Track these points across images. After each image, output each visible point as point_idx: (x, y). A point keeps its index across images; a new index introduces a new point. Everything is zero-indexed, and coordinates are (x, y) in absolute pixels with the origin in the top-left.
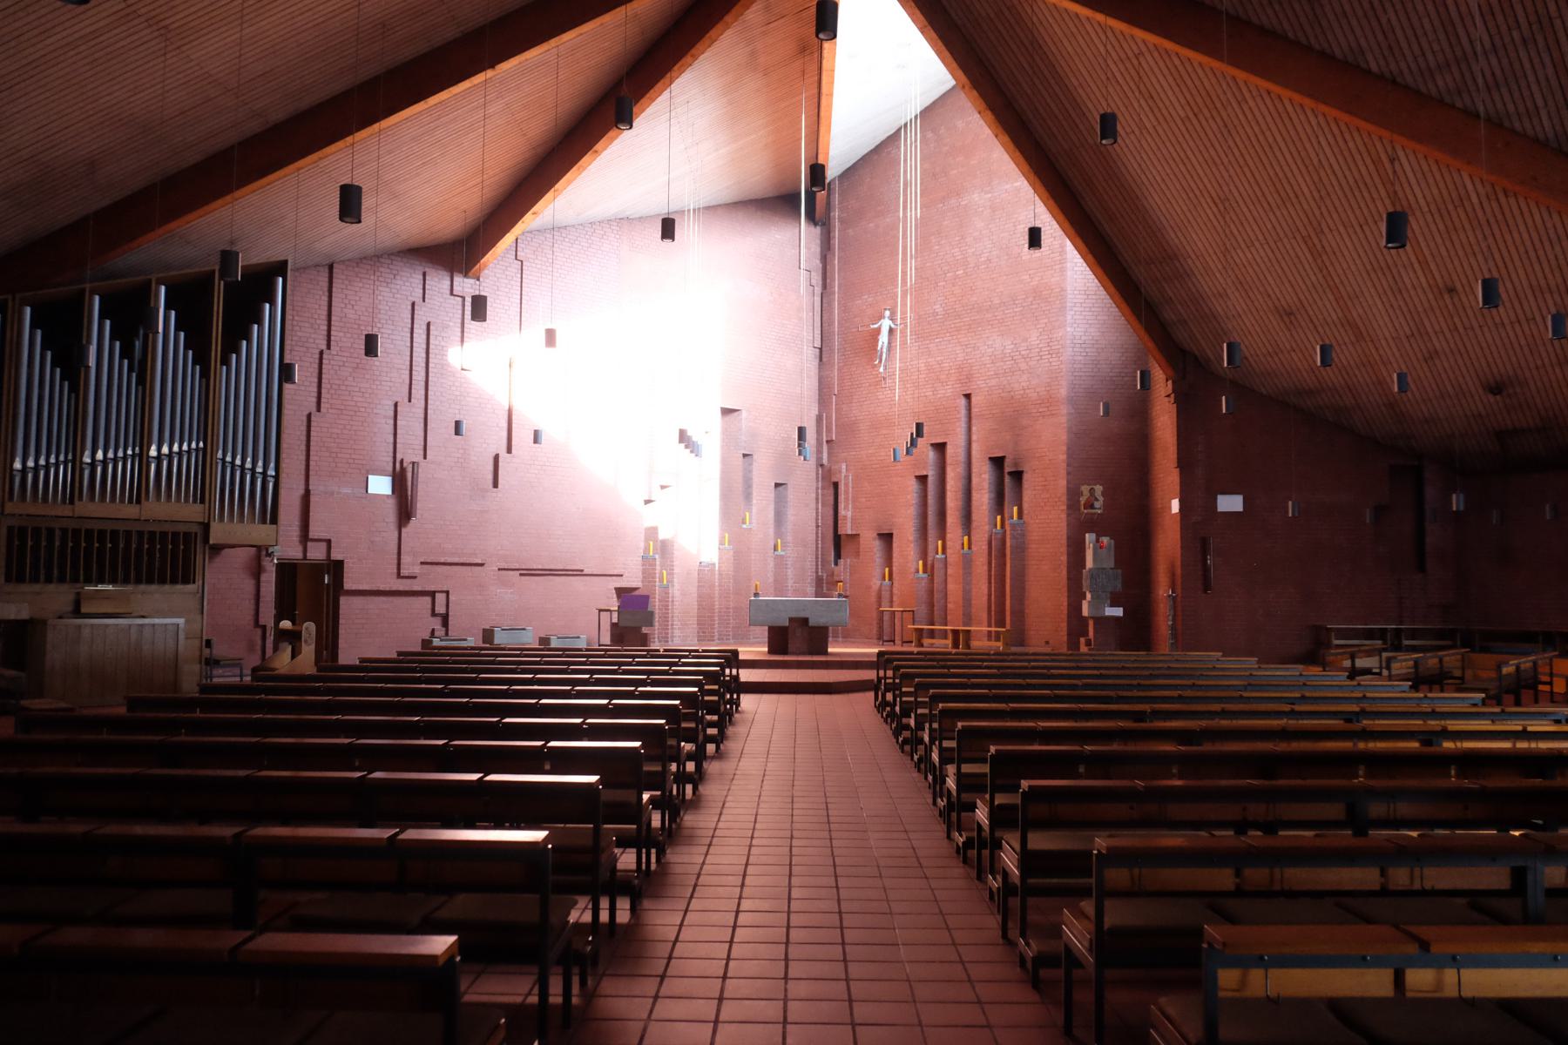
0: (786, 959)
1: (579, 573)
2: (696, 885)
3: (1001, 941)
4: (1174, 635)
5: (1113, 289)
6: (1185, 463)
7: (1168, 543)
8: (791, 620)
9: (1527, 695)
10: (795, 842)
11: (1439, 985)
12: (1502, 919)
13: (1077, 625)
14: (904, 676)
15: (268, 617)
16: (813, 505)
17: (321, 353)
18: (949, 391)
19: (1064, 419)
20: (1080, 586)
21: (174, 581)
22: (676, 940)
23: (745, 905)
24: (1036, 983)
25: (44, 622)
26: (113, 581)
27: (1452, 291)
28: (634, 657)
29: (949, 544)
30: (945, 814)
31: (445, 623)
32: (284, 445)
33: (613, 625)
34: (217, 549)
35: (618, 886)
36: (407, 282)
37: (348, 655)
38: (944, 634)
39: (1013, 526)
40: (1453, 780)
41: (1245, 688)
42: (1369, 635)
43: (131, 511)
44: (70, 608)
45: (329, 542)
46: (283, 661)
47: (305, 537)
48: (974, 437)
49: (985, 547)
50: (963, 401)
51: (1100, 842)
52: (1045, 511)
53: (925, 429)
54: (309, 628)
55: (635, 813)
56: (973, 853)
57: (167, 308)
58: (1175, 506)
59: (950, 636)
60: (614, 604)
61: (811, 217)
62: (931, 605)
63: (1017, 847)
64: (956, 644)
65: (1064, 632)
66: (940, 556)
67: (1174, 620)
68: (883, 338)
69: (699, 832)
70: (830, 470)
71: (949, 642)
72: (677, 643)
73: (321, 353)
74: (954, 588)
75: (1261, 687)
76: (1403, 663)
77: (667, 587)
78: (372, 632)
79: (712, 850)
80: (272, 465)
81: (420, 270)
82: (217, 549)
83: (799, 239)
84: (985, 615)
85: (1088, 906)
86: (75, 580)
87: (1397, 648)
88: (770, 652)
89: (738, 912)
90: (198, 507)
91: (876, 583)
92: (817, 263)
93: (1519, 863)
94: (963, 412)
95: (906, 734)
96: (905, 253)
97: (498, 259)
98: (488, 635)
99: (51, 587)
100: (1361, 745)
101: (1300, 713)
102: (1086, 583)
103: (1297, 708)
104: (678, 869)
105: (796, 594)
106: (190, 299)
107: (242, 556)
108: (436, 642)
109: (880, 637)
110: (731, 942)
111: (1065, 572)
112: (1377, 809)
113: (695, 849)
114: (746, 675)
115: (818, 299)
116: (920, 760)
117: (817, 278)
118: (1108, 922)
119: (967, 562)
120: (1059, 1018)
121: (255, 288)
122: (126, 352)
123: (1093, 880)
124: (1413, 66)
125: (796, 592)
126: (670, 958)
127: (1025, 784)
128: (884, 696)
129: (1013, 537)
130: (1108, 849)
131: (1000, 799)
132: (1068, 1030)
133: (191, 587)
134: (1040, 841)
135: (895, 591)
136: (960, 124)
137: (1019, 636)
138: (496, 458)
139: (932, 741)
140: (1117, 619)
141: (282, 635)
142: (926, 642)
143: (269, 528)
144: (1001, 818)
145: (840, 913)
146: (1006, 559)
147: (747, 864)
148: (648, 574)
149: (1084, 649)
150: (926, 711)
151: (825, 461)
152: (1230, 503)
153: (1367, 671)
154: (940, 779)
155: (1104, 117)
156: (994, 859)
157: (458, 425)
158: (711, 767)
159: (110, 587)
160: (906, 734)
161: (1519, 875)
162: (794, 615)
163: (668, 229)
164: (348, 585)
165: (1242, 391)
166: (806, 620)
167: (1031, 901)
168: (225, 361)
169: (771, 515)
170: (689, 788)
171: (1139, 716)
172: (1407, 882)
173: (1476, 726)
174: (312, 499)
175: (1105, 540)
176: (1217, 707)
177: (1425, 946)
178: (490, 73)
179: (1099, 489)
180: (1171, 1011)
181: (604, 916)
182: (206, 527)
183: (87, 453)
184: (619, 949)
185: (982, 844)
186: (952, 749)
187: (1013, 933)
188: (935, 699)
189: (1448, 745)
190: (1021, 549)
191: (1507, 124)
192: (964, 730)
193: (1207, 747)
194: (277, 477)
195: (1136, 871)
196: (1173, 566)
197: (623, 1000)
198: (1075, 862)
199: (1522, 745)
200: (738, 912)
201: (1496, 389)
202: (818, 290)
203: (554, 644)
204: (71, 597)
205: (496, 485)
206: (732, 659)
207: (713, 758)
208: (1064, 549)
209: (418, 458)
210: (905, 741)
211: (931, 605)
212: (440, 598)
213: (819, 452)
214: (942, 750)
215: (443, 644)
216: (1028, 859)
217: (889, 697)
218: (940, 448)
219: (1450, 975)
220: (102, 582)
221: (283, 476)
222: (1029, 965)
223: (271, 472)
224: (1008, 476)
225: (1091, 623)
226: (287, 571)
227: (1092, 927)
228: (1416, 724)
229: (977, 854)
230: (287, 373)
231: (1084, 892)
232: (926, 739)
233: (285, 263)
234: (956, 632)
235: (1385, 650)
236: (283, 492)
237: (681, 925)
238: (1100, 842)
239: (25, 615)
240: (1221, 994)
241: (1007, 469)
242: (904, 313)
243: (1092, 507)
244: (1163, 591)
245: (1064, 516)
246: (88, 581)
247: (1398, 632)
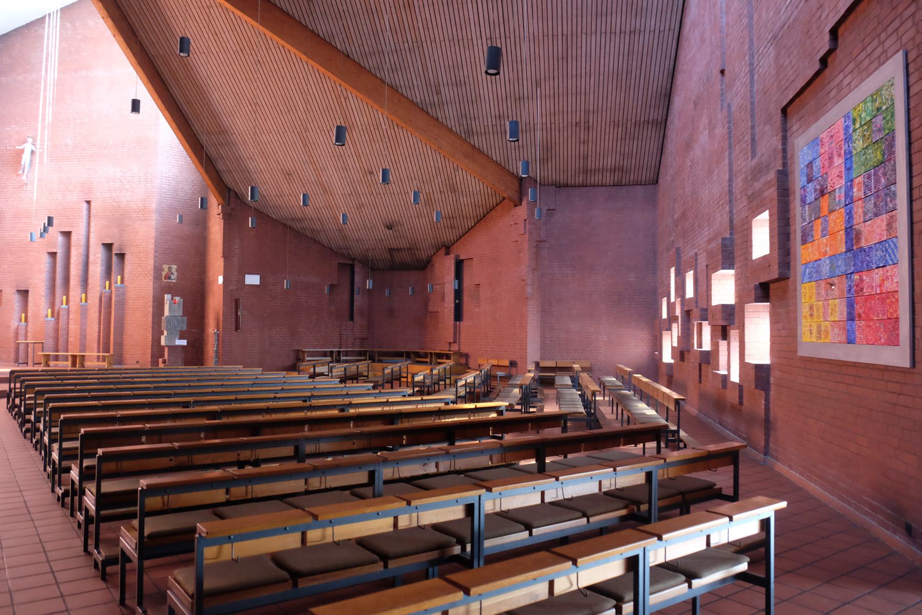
3: (83, 553)
4: (217, 356)
5: (188, 147)
6: (227, 255)
7: (216, 302)
9: (396, 383)
11: (324, 537)
12: (362, 497)
13: (157, 351)
14: (27, 387)
18: (75, 199)
19: (154, 223)
20: (160, 326)
24: (104, 577)
27: (371, 173)
29: (71, 298)
30: (51, 477)
38: (66, 358)
39: (117, 288)
40: (352, 428)
41: (252, 385)
42: (325, 354)
48: (92, 229)
49: (97, 301)
50: (85, 205)
51: (144, 482)
52: (139, 280)
53: (55, 222)
56: (68, 500)
58: (221, 280)
59: (70, 359)
62: (57, 339)
63: (94, 490)
64: (74, 364)
65: (149, 355)
66: (64, 306)
67: (218, 347)
68: (26, 157)
71: (69, 363)
74: (74, 327)
75: (261, 385)
76: (339, 370)
84: (96, 345)
85: (135, 523)
87: (338, 361)
91: (14, 324)
93: (372, 469)
94: (85, 212)
95: (28, 425)
96: (45, 101)
100: (309, 414)
101: (279, 398)
102: (164, 325)
103: (278, 396)
109: (16, 361)
111: (150, 318)
112: (310, 448)
116: (37, 442)
118: (147, 532)
119: (84, 311)
120: (117, 595)
123: (138, 508)
124: (358, 50)
127: (100, 451)
128: (14, 401)
129: (116, 296)
130: (148, 486)
131: (87, 463)
132: (122, 602)
134: (109, 486)
135: (29, 329)
136: (91, 23)
137: (119, 358)
139: (45, 429)
140: (183, 347)
142: (52, 363)
144: (85, 475)
146: (111, 311)
149: (161, 365)
150: (42, 409)
152: (253, 280)
153: (322, 374)
154: (48, 453)
155: (182, 39)
156: (81, 501)
160: (28, 425)
161: (372, 475)
165: (261, 215)
167: (103, 525)
171: (186, 405)
172: (318, 485)
173: (367, 400)
175: (177, 299)
176: (233, 397)
177: (315, 517)
179: (174, 267)
180: (180, 578)
181: (498, 501)
185: (74, 493)
186: (56, 433)
187: (91, 548)
188: (48, 400)
189: (352, 411)
190: (122, 303)
191: (400, 90)
192: (65, 420)
193: (224, 420)
195: (166, 497)
196: (218, 315)
198: (128, 497)
199: (386, 409)
201: (390, 227)
208: (151, 304)
210: (27, 431)
211: (57, 339)
214: (50, 434)
216: (103, 500)
217: (17, 401)
218: (67, 235)
219: (329, 530)
222: (100, 566)
224: (115, 255)
225: (166, 349)
227: (137, 534)
228: (339, 401)
229: (70, 499)
231: (132, 516)
232: (42, 427)
234: (74, 357)
235: (331, 362)
238: (144, 482)
240: (205, 562)
241: (115, 251)
242: (42, 141)
243: (169, 278)
244: (211, 329)
245: (151, 283)
247: (339, 352)
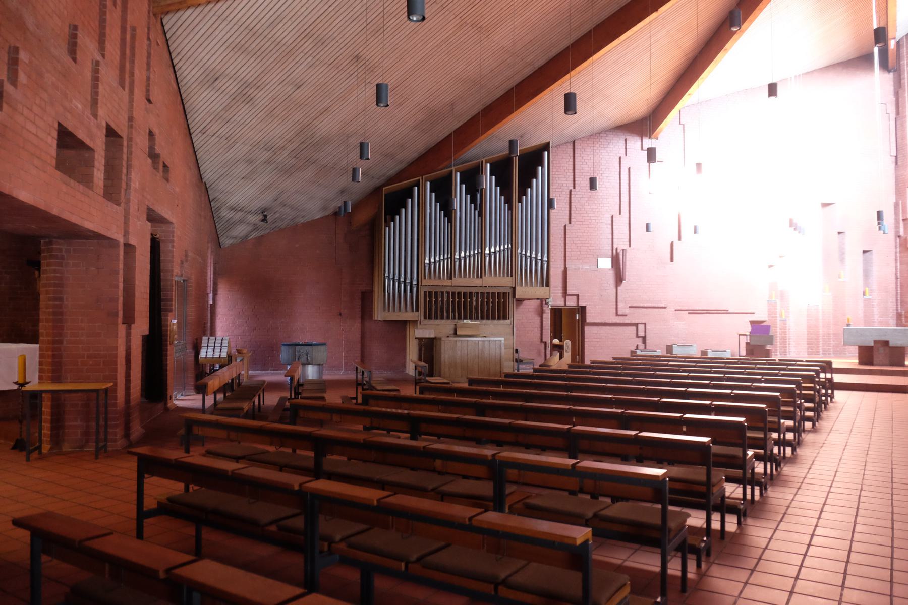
0: (845, 573)
1: (726, 312)
2: (785, 514)
8: (875, 342)
10: (863, 493)
15: (547, 337)
16: (893, 264)
17: (570, 191)
21: (499, 318)
22: (766, 548)
23: (819, 531)
25: (440, 339)
26: (471, 318)
28: (745, 368)
31: (644, 342)
32: (551, 244)
33: (747, 344)
34: (520, 301)
35: (725, 507)
36: (617, 145)
37: (590, 357)
43: (477, 282)
44: (452, 332)
45: (578, 296)
46: (555, 362)
47: (565, 294)
54: (567, 344)
55: (741, 463)
57: (461, 183)
60: (748, 329)
61: (884, 65)
69: (792, 479)
70: (906, 240)
72: (792, 355)
73: (570, 191)
77: (785, 320)
78: (603, 346)
79: (800, 492)
80: (546, 255)
81: (624, 137)
82: (520, 301)
83: (878, 81)
86: (454, 318)
88: (860, 363)
89: (813, 535)
90: (510, 279)
92: (892, 98)
97: (669, 124)
98: (669, 349)
99: (443, 321)
104: (774, 501)
105: (881, 323)
106: (501, 169)
107: (534, 304)
108: (639, 353)
110: (805, 555)
113: (787, 490)
114: (838, 378)
115: (893, 123)
117: (892, 109)
121: (533, 159)
122: (473, 200)
125: (881, 323)
126: (760, 559)
133: (507, 321)
138: (672, 244)
141: (555, 347)
143: (545, 289)
145: (892, 547)
147: (824, 504)
148: (772, 312)
151: (902, 233)
157: (648, 225)
158: (807, 437)
159: (469, 321)
162: (877, 339)
163: (772, 90)
164: (588, 320)
166: (886, 343)
168: (520, 201)
170: (789, 450)
174: (568, 272)
178: (654, 15)
182: (514, 289)
183: (487, 249)
184: (721, 548)
194: (548, 261)
197: (724, 580)
200: (813, 535)
202: (893, 116)
203: (710, 355)
204: (453, 326)
205: (672, 260)
206: (827, 367)
207: (809, 431)
209: (626, 247)
212: (641, 327)
213: (897, 227)
215: (643, 354)
220: (466, 318)
221: (551, 260)
223: (545, 259)
226: (557, 313)
230: (551, 204)
233: (549, 143)
236: (552, 269)
237: (771, 538)
239: (432, 336)
246: (460, 318)
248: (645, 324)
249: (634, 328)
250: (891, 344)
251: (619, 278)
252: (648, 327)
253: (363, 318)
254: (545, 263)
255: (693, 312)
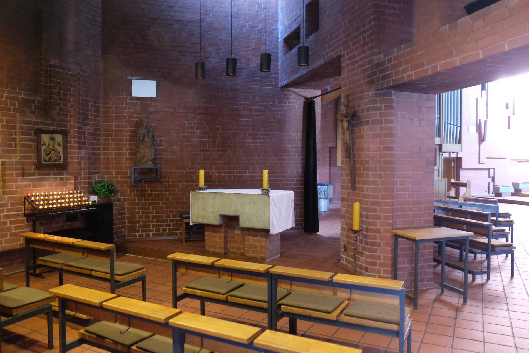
164: (463, 166)
169: (128, 286)
194: (461, 127)
212: (492, 171)
236: (463, 132)
248: (494, 169)
249: (487, 171)
250: (244, 223)
251: (481, 140)
252: (496, 171)
253: (330, 165)
254: (459, 128)
255: (520, 161)
